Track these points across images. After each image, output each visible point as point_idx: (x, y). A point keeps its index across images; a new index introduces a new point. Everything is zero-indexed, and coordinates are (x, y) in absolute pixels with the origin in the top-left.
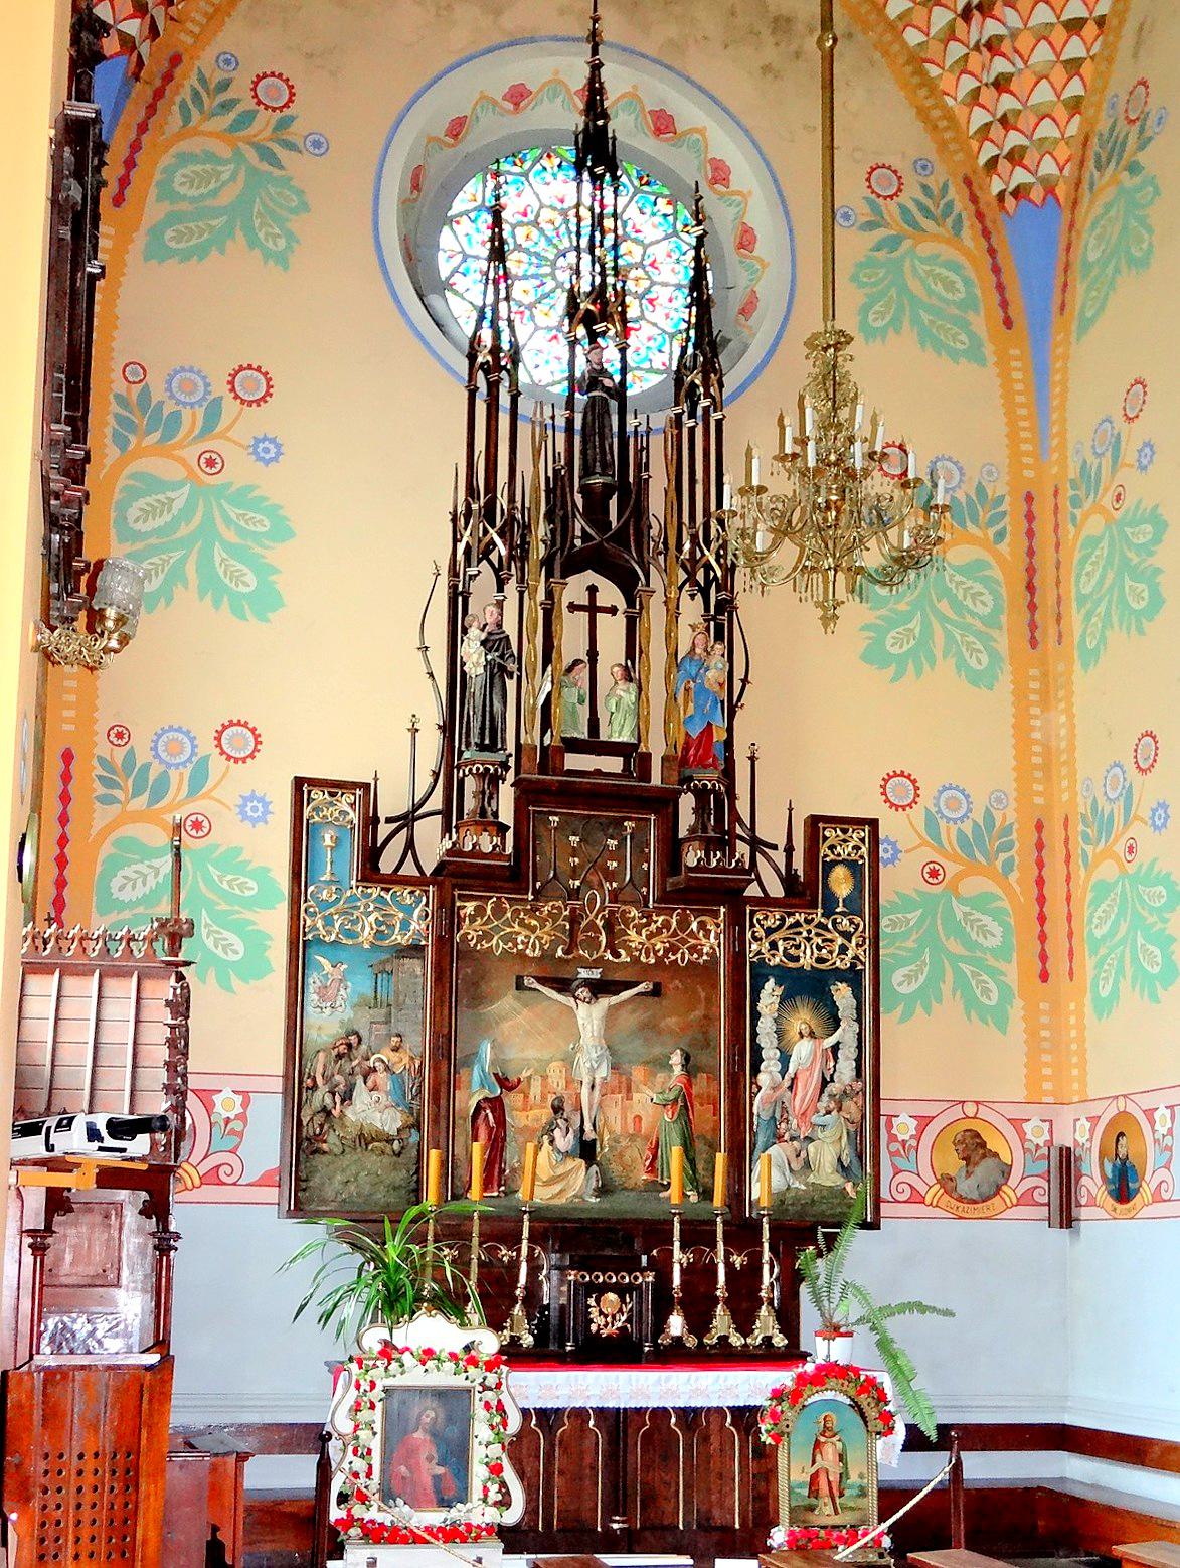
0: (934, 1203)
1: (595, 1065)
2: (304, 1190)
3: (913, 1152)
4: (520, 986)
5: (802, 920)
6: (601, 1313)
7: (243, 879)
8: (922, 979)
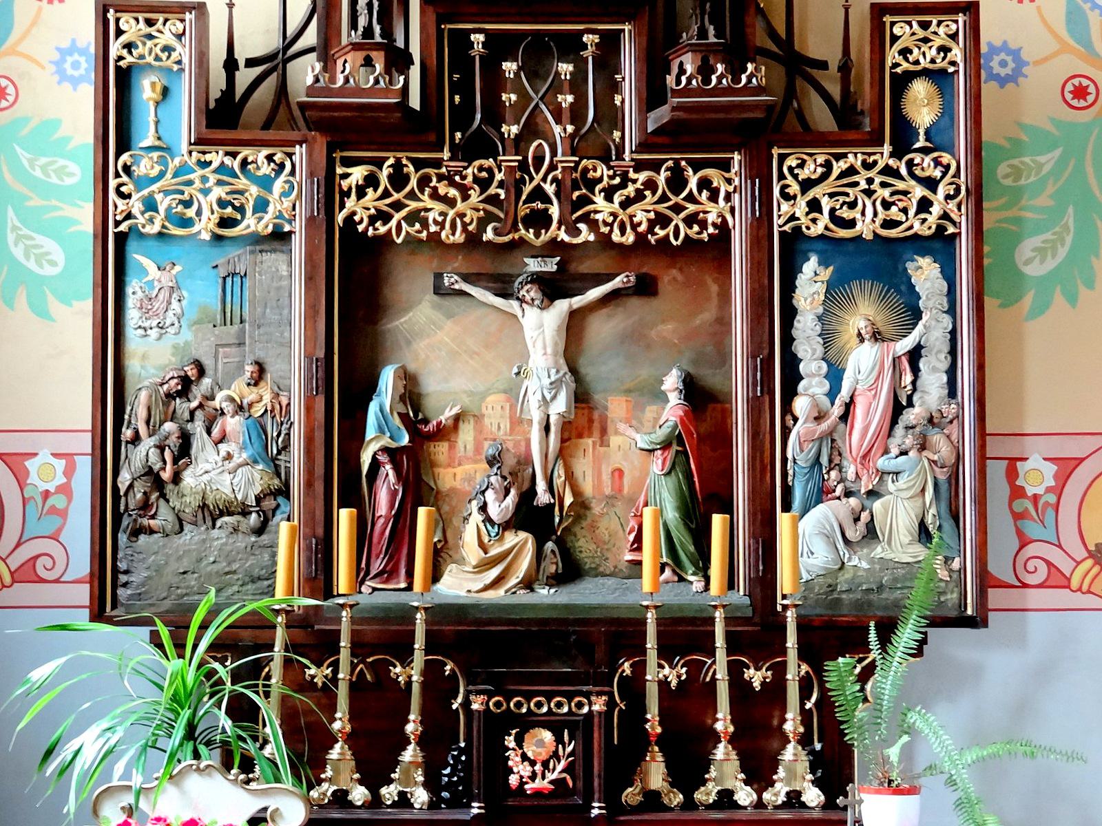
0: (1085, 588)
1: (548, 397)
2: (125, 585)
3: (1050, 513)
4: (439, 290)
5: (858, 164)
6: (524, 757)
7: (62, 162)
8: (1062, 252)
